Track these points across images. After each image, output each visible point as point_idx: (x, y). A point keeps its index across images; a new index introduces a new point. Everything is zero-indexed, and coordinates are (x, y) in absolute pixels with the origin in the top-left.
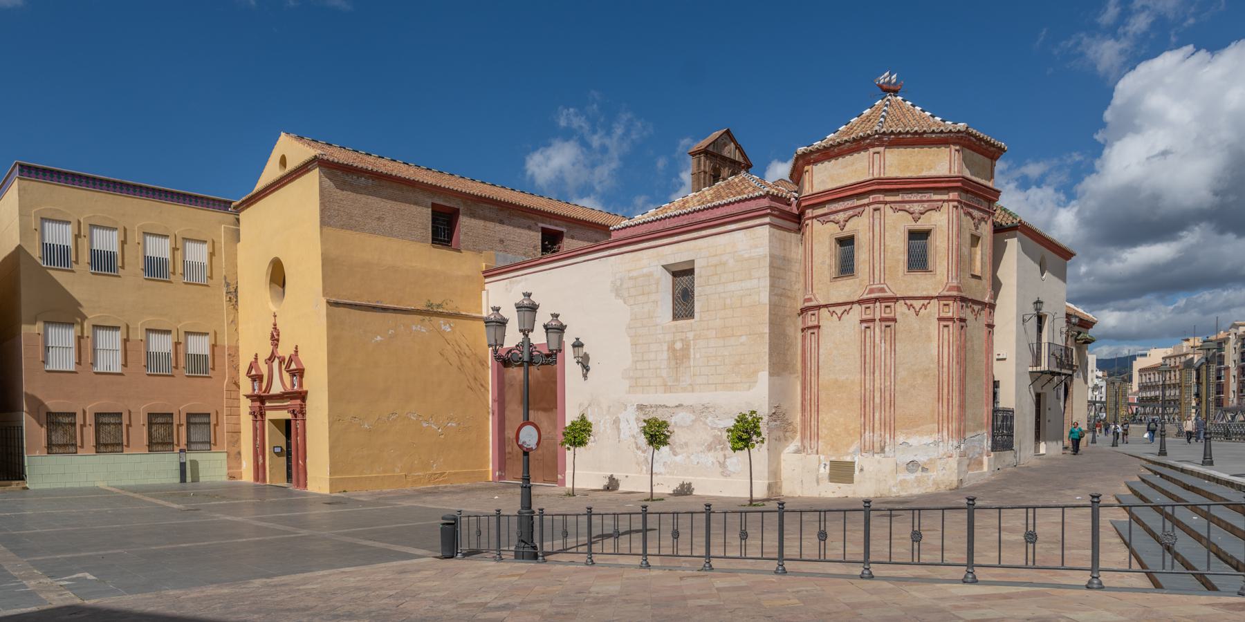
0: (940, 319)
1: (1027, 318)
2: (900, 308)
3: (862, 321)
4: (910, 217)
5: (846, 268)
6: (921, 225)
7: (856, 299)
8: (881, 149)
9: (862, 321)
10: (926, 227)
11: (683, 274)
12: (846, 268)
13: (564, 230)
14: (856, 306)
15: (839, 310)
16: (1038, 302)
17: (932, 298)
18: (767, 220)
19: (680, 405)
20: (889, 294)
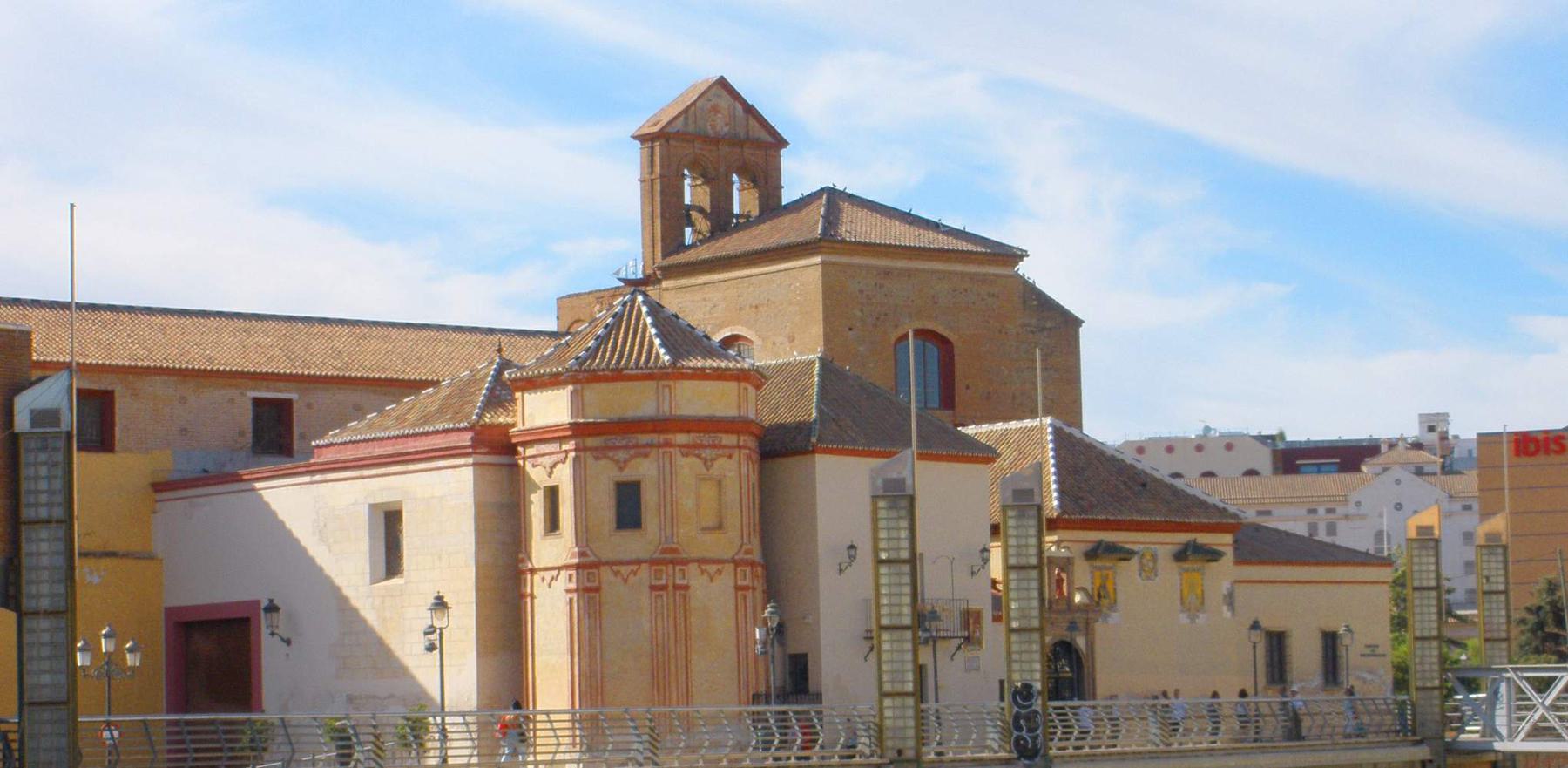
0: (653, 588)
2: (606, 573)
3: (568, 591)
5: (553, 524)
6: (628, 475)
7: (560, 563)
10: (633, 479)
11: (390, 521)
13: (293, 396)
14: (563, 572)
15: (548, 575)
16: (852, 547)
17: (639, 562)
18: (470, 460)
19: (391, 696)
20: (592, 558)
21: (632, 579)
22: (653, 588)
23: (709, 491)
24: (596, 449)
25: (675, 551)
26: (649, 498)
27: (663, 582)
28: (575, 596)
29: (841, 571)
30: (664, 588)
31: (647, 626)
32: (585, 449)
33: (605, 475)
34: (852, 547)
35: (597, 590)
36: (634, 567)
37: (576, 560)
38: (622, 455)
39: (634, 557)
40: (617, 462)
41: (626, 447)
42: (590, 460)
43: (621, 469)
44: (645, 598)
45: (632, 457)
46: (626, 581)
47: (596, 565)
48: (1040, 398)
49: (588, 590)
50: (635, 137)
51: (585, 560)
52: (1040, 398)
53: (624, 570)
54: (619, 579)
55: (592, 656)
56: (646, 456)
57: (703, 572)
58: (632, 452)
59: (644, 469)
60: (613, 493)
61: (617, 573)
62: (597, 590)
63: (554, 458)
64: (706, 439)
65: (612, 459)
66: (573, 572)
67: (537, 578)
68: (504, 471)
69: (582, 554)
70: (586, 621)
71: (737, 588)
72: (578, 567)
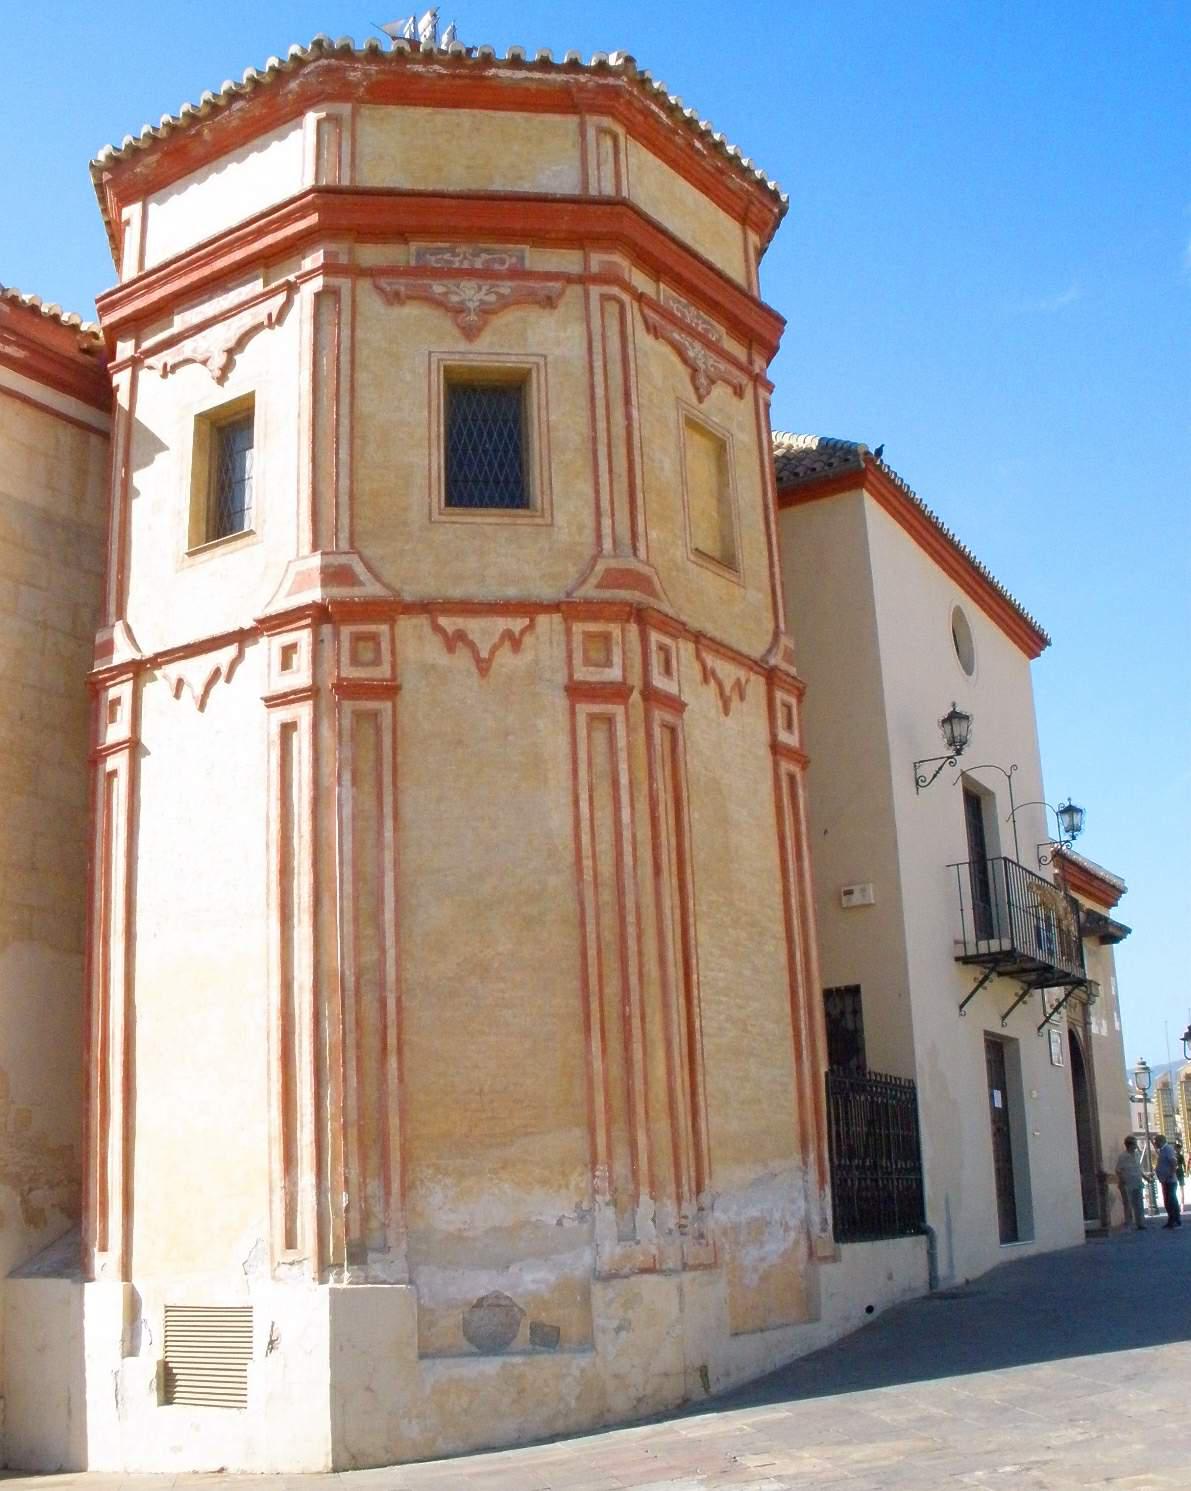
0: (577, 692)
1: (927, 770)
3: (274, 701)
4: (446, 324)
5: (221, 513)
8: (345, 109)
9: (274, 701)
10: (511, 362)
12: (221, 513)
15: (196, 670)
16: (954, 717)
17: (528, 608)
20: (371, 589)
21: (505, 659)
22: (577, 692)
23: (702, 468)
24: (391, 271)
25: (641, 582)
26: (557, 424)
27: (614, 674)
28: (303, 713)
29: (917, 782)
30: (618, 692)
31: (560, 820)
32: (357, 272)
33: (415, 355)
34: (954, 717)
35: (389, 690)
36: (517, 624)
37: (314, 594)
38: (470, 293)
39: (511, 592)
40: (459, 310)
41: (486, 274)
42: (371, 303)
43: (470, 333)
44: (550, 726)
45: (505, 303)
46: (483, 666)
47: (388, 609)
48: (329, 1159)
49: (348, 690)
50: (262, 698)
51: (341, 592)
52: (329, 1159)
53: (483, 630)
54: (462, 660)
55: (367, 915)
56: (549, 302)
57: (707, 675)
58: (506, 288)
59: (547, 344)
60: (439, 401)
61: (455, 641)
62: (389, 690)
63: (246, 320)
64: (693, 315)
65: (439, 303)
66: (303, 637)
67: (156, 691)
68: (67, 436)
69: (333, 575)
70: (341, 794)
71: (776, 748)
72: (319, 615)
